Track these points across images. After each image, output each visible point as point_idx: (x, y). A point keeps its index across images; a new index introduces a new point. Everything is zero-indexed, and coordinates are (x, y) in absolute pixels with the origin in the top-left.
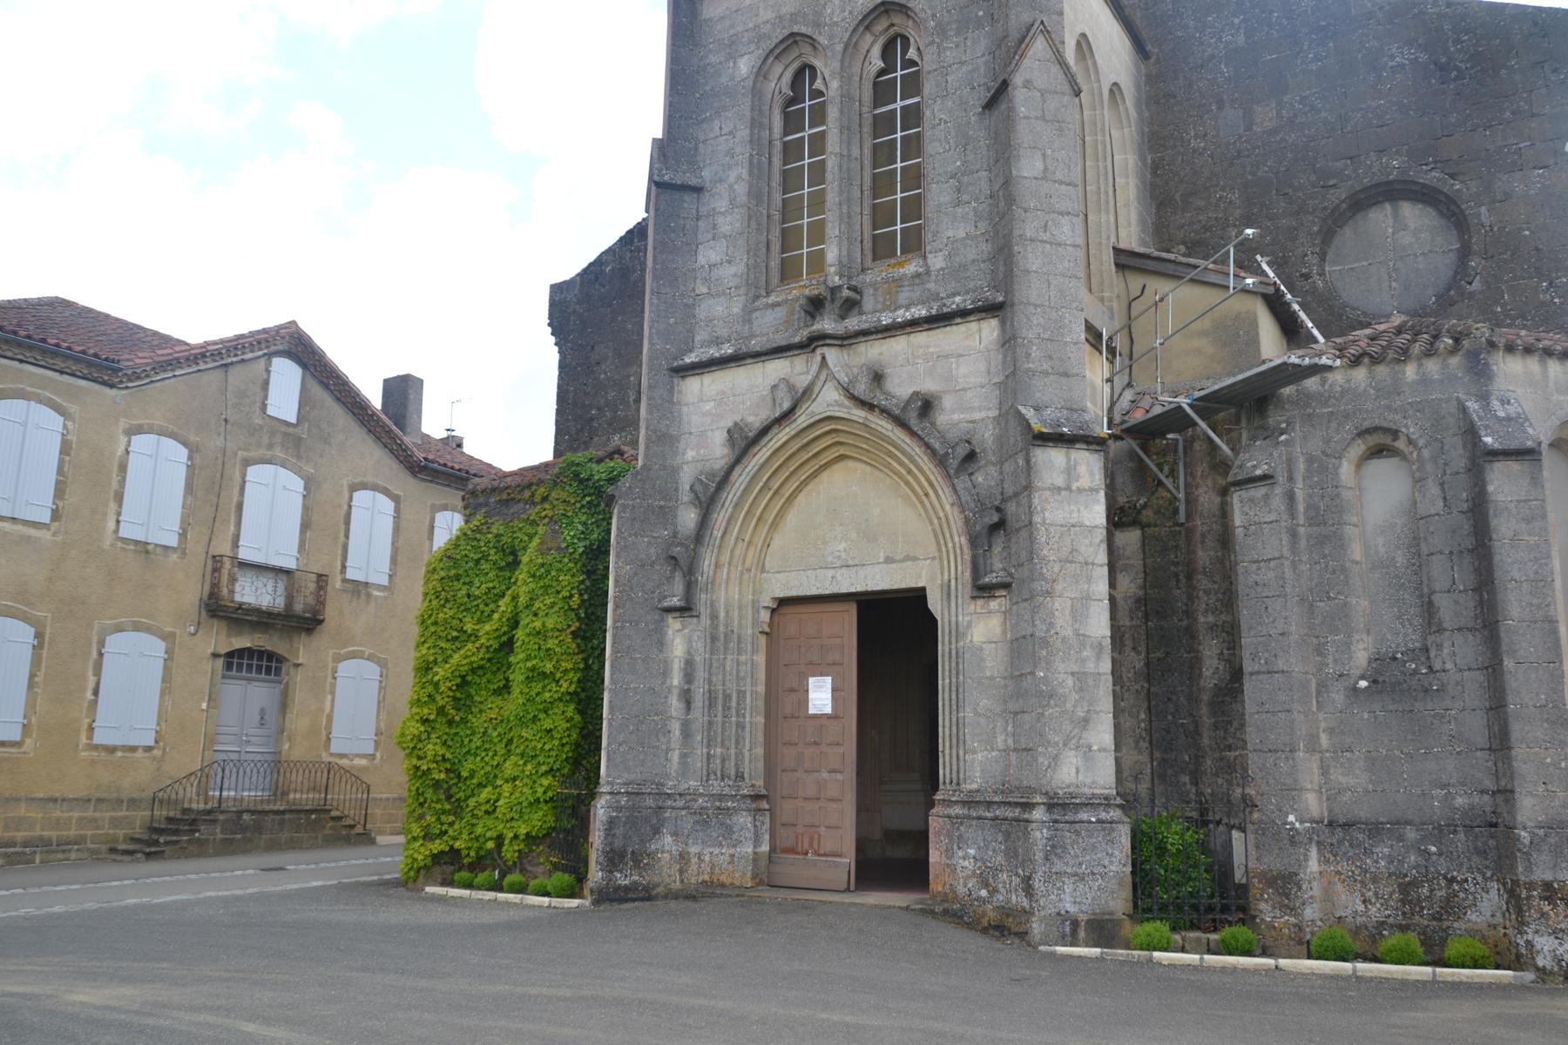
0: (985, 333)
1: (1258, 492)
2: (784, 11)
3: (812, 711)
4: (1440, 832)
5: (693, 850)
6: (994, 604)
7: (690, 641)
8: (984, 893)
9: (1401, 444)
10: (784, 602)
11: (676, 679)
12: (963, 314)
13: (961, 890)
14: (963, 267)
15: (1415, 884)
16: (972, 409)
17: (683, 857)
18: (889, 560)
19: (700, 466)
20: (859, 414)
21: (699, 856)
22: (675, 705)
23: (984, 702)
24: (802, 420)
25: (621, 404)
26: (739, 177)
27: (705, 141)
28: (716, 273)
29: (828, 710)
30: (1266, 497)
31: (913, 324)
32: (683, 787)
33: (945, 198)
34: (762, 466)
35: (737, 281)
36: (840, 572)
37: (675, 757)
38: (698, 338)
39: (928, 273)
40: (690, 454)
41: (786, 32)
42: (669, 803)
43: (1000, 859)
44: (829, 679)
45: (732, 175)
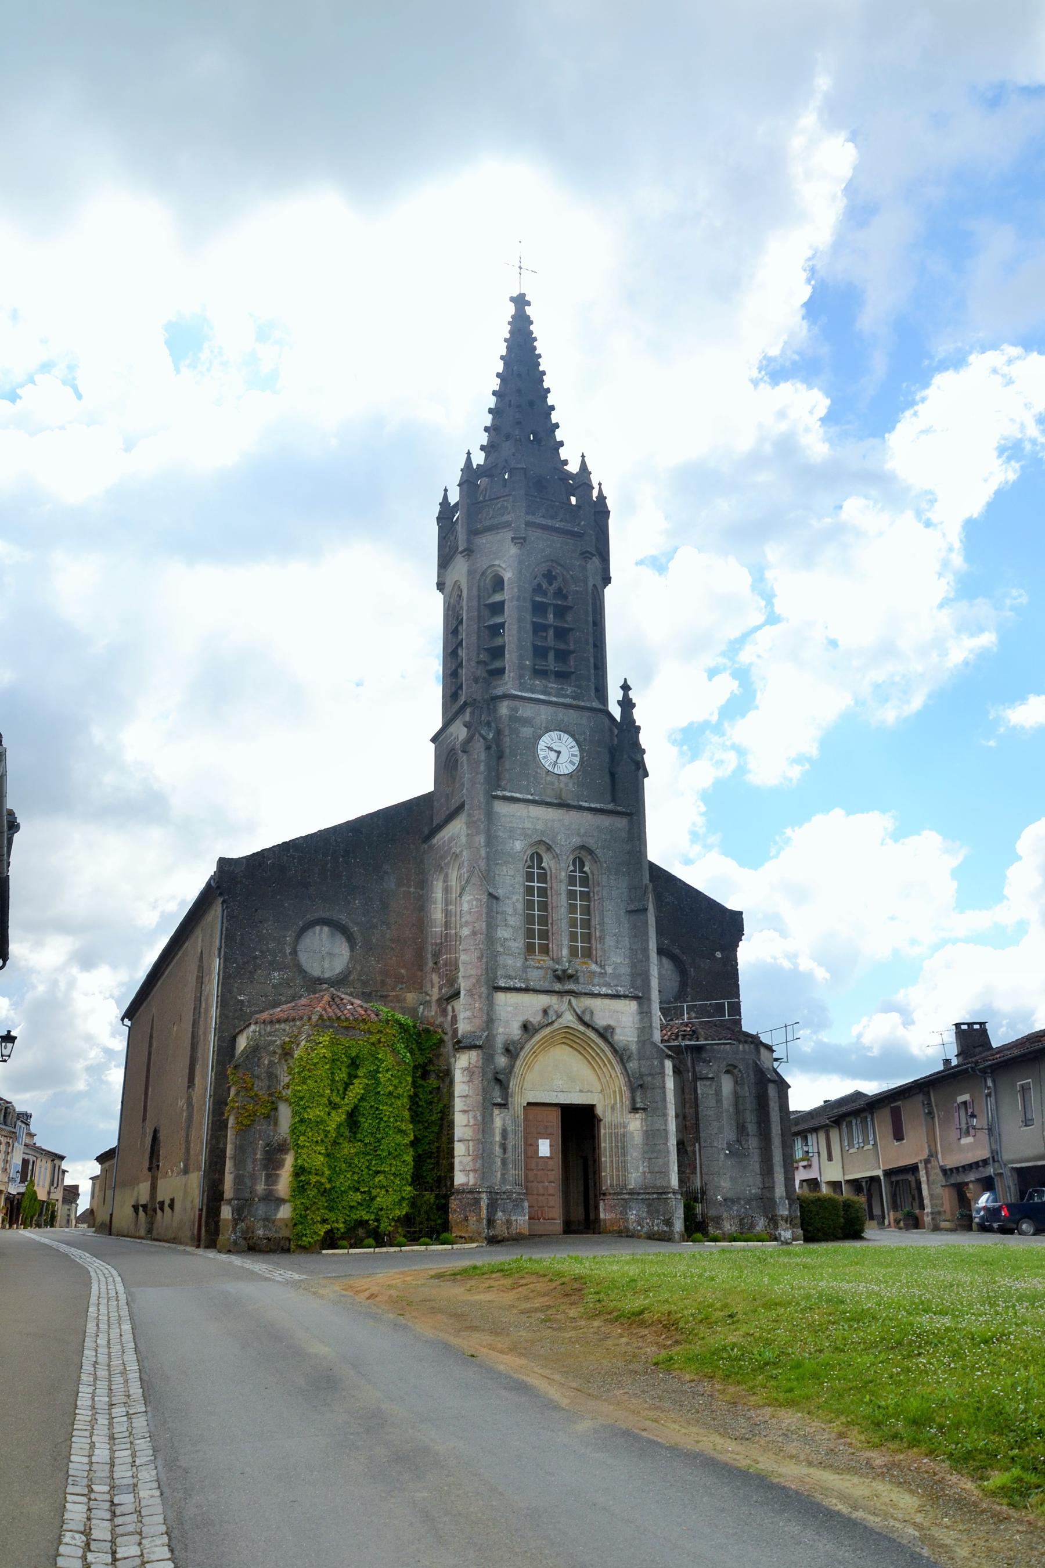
0: (632, 1005)
1: (708, 1083)
2: (538, 827)
3: (540, 1155)
4: (749, 1201)
5: (513, 1218)
6: (637, 1116)
7: (504, 1120)
8: (639, 1228)
9: (736, 1071)
10: (529, 1104)
11: (498, 1138)
12: (625, 997)
13: (631, 1227)
14: (620, 975)
15: (743, 1219)
16: (627, 1036)
17: (509, 1222)
18: (581, 1091)
19: (506, 1036)
20: (582, 1028)
21: (516, 1220)
22: (498, 1150)
23: (635, 1154)
24: (556, 1025)
25: (279, 953)
26: (518, 900)
27: (499, 875)
28: (508, 943)
29: (548, 1155)
30: (710, 1085)
31: (606, 996)
32: (504, 1189)
33: (612, 944)
34: (538, 1042)
35: (517, 951)
36: (559, 1094)
37: (499, 1175)
38: (499, 973)
39: (606, 973)
40: (501, 1030)
41: (539, 838)
42: (498, 1197)
43: (645, 1215)
44: (548, 1141)
45: (515, 898)
